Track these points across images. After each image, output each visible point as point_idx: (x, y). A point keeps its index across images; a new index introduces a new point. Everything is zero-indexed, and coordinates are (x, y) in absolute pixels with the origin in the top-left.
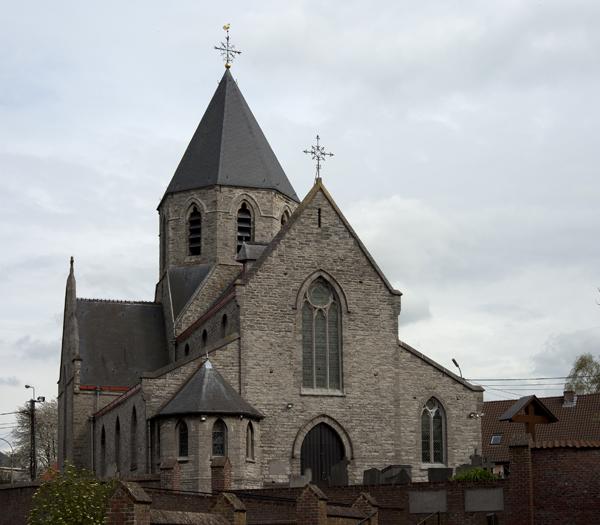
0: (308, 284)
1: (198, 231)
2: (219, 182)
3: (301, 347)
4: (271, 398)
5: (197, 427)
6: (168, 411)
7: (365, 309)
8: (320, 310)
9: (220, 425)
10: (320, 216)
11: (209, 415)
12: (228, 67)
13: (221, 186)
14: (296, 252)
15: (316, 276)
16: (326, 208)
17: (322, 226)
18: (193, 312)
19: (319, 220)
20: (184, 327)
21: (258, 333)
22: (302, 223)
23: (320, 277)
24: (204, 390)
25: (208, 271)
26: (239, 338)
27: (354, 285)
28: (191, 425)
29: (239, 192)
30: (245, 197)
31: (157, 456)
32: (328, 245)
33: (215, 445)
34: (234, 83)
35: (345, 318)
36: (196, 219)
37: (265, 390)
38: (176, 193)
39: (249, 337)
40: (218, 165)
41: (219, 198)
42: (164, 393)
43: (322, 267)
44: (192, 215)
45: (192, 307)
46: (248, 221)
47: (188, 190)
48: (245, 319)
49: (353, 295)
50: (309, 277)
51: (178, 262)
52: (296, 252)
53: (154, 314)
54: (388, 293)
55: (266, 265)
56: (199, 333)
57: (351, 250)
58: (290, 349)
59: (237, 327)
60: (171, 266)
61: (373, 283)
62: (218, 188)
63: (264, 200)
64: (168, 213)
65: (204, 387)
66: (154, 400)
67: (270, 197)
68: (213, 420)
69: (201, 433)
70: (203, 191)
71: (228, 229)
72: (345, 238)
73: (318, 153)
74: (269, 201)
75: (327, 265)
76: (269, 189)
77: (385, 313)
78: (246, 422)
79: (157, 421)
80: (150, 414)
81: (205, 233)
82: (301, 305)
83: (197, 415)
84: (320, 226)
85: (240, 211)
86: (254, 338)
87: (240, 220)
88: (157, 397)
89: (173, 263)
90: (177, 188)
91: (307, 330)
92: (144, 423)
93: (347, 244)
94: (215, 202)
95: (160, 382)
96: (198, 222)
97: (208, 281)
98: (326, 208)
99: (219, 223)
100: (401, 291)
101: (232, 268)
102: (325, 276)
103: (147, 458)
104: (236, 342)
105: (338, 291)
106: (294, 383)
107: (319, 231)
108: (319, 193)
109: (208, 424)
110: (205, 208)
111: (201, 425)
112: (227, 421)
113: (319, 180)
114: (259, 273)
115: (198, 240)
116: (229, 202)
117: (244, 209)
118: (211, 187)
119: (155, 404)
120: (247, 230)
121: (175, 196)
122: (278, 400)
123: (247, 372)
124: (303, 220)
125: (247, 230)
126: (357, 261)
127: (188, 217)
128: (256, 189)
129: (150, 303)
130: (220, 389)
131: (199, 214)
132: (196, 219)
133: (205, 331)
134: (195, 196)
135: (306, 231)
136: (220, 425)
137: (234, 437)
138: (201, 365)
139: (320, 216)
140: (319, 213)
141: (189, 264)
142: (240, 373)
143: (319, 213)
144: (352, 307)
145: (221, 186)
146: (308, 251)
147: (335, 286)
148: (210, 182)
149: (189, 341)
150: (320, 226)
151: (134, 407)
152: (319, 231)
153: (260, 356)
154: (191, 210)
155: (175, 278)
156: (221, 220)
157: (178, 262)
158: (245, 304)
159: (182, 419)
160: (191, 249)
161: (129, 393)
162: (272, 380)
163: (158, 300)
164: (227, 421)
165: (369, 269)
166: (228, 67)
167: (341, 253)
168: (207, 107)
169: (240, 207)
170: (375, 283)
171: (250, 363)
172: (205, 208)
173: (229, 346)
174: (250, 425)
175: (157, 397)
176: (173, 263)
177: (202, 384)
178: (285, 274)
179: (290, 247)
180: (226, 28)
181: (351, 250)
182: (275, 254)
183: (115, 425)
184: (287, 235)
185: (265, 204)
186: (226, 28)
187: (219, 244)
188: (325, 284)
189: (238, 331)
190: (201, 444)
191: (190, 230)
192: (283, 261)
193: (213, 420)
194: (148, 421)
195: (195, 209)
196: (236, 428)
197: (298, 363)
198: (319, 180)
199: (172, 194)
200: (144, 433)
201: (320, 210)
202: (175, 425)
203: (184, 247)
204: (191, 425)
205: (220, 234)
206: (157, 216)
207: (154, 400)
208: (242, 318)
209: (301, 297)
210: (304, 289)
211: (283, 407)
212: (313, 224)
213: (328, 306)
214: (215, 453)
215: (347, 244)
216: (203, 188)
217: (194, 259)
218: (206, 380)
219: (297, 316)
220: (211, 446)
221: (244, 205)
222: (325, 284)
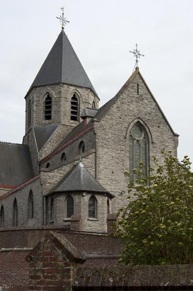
0: (132, 125)
1: (50, 107)
2: (62, 82)
3: (128, 160)
4: (112, 188)
5: (80, 199)
6: (59, 189)
7: (161, 142)
8: (138, 141)
9: (93, 199)
10: (138, 88)
11: (88, 192)
12: (63, 28)
13: (63, 84)
14: (126, 106)
15: (136, 121)
16: (141, 84)
17: (139, 93)
18: (48, 149)
19: (138, 90)
20: (44, 156)
21: (106, 150)
22: (129, 91)
23: (138, 122)
24: (82, 178)
25: (56, 128)
26: (96, 152)
27: (155, 128)
28: (76, 198)
29: (72, 88)
30: (75, 91)
31: (50, 218)
32: (143, 104)
33: (89, 211)
34: (65, 34)
35: (151, 146)
36: (49, 102)
37: (109, 183)
38: (38, 87)
39: (101, 152)
40: (61, 74)
41: (62, 90)
42: (53, 181)
43: (139, 116)
44: (46, 99)
45: (48, 146)
46: (76, 104)
47: (45, 86)
48: (99, 142)
49: (155, 133)
50: (133, 121)
51: (39, 123)
52: (126, 106)
53: (25, 150)
54: (172, 134)
55: (110, 112)
56: (59, 156)
57: (154, 109)
58: (123, 161)
59: (94, 145)
60: (34, 125)
61: (165, 128)
62: (62, 84)
63: (85, 94)
64: (33, 98)
65: (82, 176)
66: (48, 185)
67: (87, 92)
68: (90, 196)
69: (82, 203)
70: (53, 86)
71: (66, 107)
72: (151, 102)
73: (137, 54)
74: (87, 94)
75: (142, 116)
76: (87, 88)
77: (171, 145)
78: (106, 198)
79: (51, 196)
80: (45, 193)
81: (54, 108)
82: (128, 137)
83: (80, 192)
84: (138, 94)
85: (72, 98)
86: (104, 153)
87: (72, 103)
88: (49, 183)
89: (36, 124)
90: (39, 84)
91: (132, 152)
92: (41, 198)
93: (152, 105)
94: (60, 92)
95: (50, 174)
96: (50, 102)
97: (56, 133)
98: (141, 84)
99: (62, 103)
100: (179, 134)
101: (69, 127)
102: (141, 122)
103: (43, 220)
104: (94, 154)
105: (148, 130)
106: (125, 180)
107: (138, 96)
108: (138, 75)
109: (87, 198)
110: (54, 95)
111: (82, 198)
112: (97, 197)
113: (137, 69)
114: (106, 116)
115: (50, 112)
116: (68, 92)
117: (74, 98)
118: (58, 84)
119: (48, 187)
120: (76, 108)
121: (37, 89)
122: (116, 189)
123: (100, 172)
124: (129, 89)
125: (76, 108)
126: (157, 115)
127: (44, 100)
128: (81, 87)
129: (21, 145)
130: (91, 180)
131: (50, 98)
132: (49, 102)
133: (64, 154)
134: (49, 88)
135: (131, 95)
136: (93, 199)
137: (101, 207)
138: (75, 166)
139: (138, 88)
140: (138, 86)
141: (45, 124)
142: (96, 172)
143: (138, 86)
144: (155, 140)
145: (63, 84)
146: (132, 107)
147: (146, 127)
148: (57, 82)
149: (49, 162)
150: (138, 94)
151: (15, 198)
152: (138, 96)
153: (107, 164)
154: (46, 96)
155: (37, 131)
156: (63, 101)
157: (39, 123)
158: (99, 133)
159: (69, 195)
160: (45, 116)
161: (15, 190)
162: (113, 177)
163: (25, 144)
164: (97, 197)
165: (163, 120)
166: (63, 28)
167: (149, 109)
168: (53, 45)
169: (72, 96)
170: (166, 128)
171: (102, 167)
172: (54, 95)
173: (90, 156)
174: (108, 201)
175: (49, 183)
176: (36, 124)
177: (80, 174)
178: (120, 118)
179: (123, 103)
180: (62, 9)
181: (154, 109)
182: (115, 106)
183: (13, 201)
184: (121, 96)
185: (84, 96)
186: (62, 9)
187: (62, 114)
188: (140, 126)
189: (95, 148)
190: (82, 210)
191: (46, 107)
192: (119, 110)
193: (90, 196)
194: (43, 197)
195: (48, 96)
196: (101, 200)
197: (127, 169)
198: (137, 69)
199: (36, 87)
200: (41, 205)
201: (138, 84)
202: (65, 198)
203: (42, 115)
204: (76, 198)
205: (62, 109)
206: (24, 102)
207: (47, 185)
208: (97, 140)
209: (128, 132)
210: (130, 127)
211: (119, 194)
212: (135, 92)
213: (141, 138)
214: (90, 216)
215: (152, 105)
216: (54, 84)
217: (47, 121)
218: (82, 173)
219: (126, 142)
220: (88, 211)
221: (74, 95)
222: (140, 126)
